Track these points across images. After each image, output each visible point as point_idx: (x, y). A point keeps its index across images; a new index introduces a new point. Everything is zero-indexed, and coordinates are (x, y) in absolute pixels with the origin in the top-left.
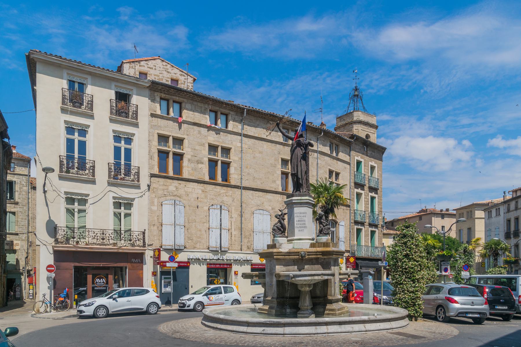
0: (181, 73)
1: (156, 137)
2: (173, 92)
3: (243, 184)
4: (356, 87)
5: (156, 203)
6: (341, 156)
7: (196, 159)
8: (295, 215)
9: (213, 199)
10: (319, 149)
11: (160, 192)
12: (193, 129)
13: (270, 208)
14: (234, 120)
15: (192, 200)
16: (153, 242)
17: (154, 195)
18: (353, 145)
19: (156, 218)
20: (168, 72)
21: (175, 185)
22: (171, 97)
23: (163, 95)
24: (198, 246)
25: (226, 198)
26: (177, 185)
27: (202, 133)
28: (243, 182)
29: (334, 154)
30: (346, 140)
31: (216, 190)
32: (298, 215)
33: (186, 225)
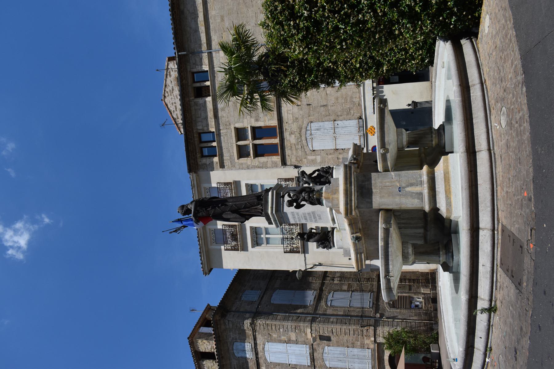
0: (168, 76)
5: (313, 157)
11: (300, 153)
15: (301, 112)
17: (304, 160)
19: (330, 157)
20: (173, 89)
21: (288, 136)
23: (199, 155)
24: (356, 100)
33: (332, 118)
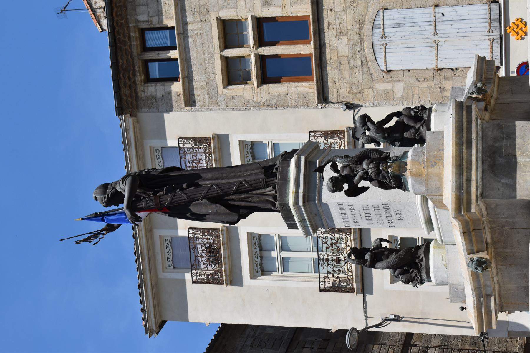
5: (387, 86)
11: (359, 76)
17: (366, 91)
19: (424, 85)
21: (333, 39)
22: (136, 59)
23: (140, 78)
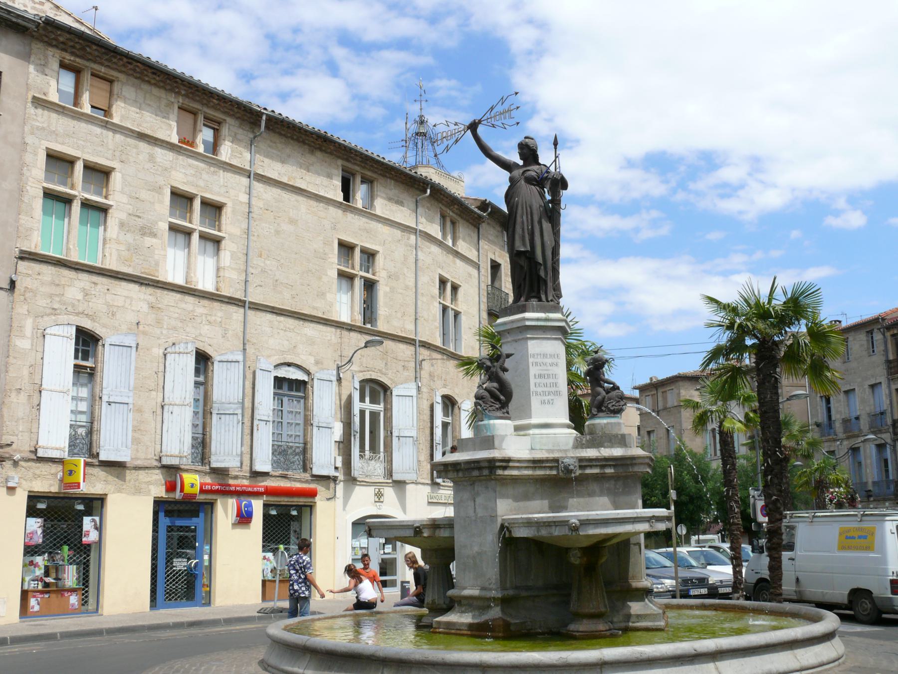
1: (42, 157)
2: (96, 53)
3: (248, 293)
4: (421, 116)
6: (463, 247)
7: (140, 222)
8: (531, 360)
9: (175, 329)
10: (420, 227)
11: (42, 302)
12: (136, 147)
13: (312, 360)
14: (235, 140)
16: (13, 439)
17: (26, 307)
18: (484, 227)
21: (82, 284)
25: (207, 327)
26: (87, 285)
27: (158, 160)
28: (250, 289)
29: (449, 243)
30: (473, 211)
31: (183, 305)
32: (539, 360)
